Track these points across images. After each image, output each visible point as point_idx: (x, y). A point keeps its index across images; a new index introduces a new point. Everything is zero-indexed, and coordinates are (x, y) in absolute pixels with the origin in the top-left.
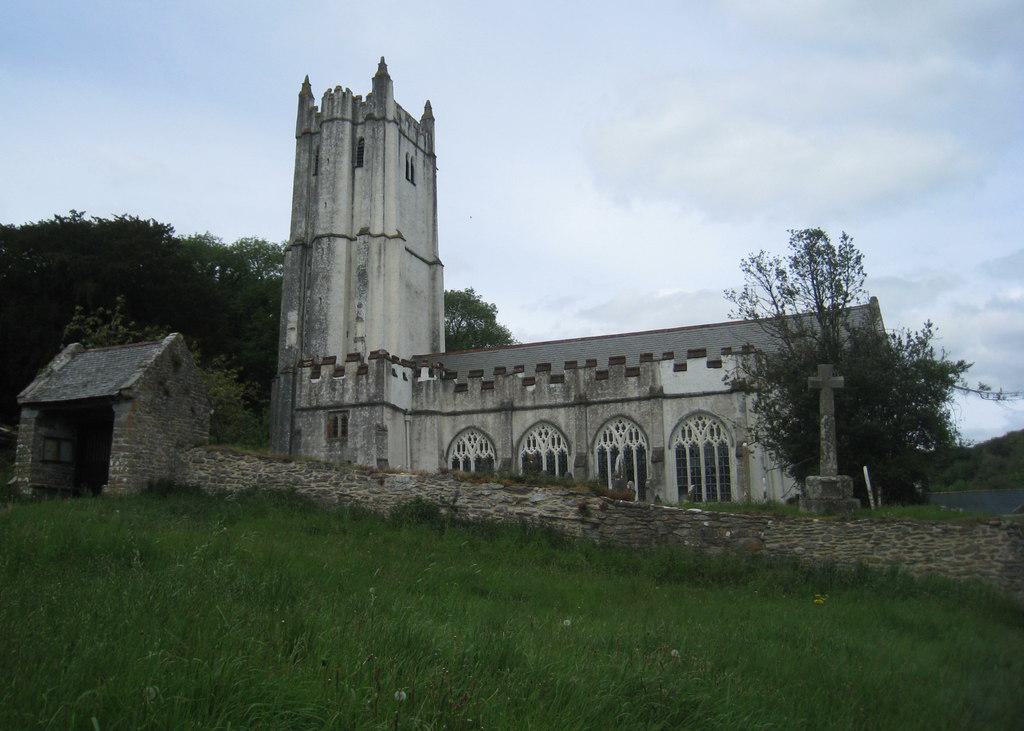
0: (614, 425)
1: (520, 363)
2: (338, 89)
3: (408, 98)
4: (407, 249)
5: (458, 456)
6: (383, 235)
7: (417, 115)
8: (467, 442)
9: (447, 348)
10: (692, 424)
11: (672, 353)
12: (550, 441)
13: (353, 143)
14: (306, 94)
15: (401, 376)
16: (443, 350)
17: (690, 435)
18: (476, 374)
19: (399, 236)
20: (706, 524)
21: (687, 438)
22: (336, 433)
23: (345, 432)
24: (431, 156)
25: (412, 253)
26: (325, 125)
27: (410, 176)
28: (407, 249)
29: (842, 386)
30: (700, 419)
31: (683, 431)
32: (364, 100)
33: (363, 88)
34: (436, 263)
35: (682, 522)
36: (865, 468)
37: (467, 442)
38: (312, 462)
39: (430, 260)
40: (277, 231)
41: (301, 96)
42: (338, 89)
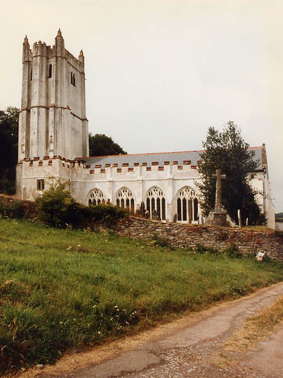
0: (185, 190)
1: (116, 163)
2: (40, 42)
3: (72, 47)
4: (71, 113)
5: (180, 197)
6: (61, 108)
7: (76, 55)
8: (94, 193)
9: (91, 155)
10: (184, 190)
11: (190, 161)
12: (158, 194)
13: (47, 67)
14: (26, 45)
15: (66, 166)
16: (88, 156)
17: (183, 195)
18: (126, 165)
19: (68, 108)
20: (168, 227)
21: (182, 196)
22: (40, 188)
23: (43, 185)
24: (83, 73)
25: (74, 115)
26: (34, 58)
27: (73, 82)
28: (71, 113)
29: (225, 178)
30: (187, 188)
31: (180, 193)
32: (51, 48)
33: (51, 43)
34: (84, 120)
35: (159, 226)
36: (239, 211)
37: (94, 193)
38: (20, 197)
39: (83, 118)
40: (17, 103)
41: (24, 44)
42: (40, 42)
